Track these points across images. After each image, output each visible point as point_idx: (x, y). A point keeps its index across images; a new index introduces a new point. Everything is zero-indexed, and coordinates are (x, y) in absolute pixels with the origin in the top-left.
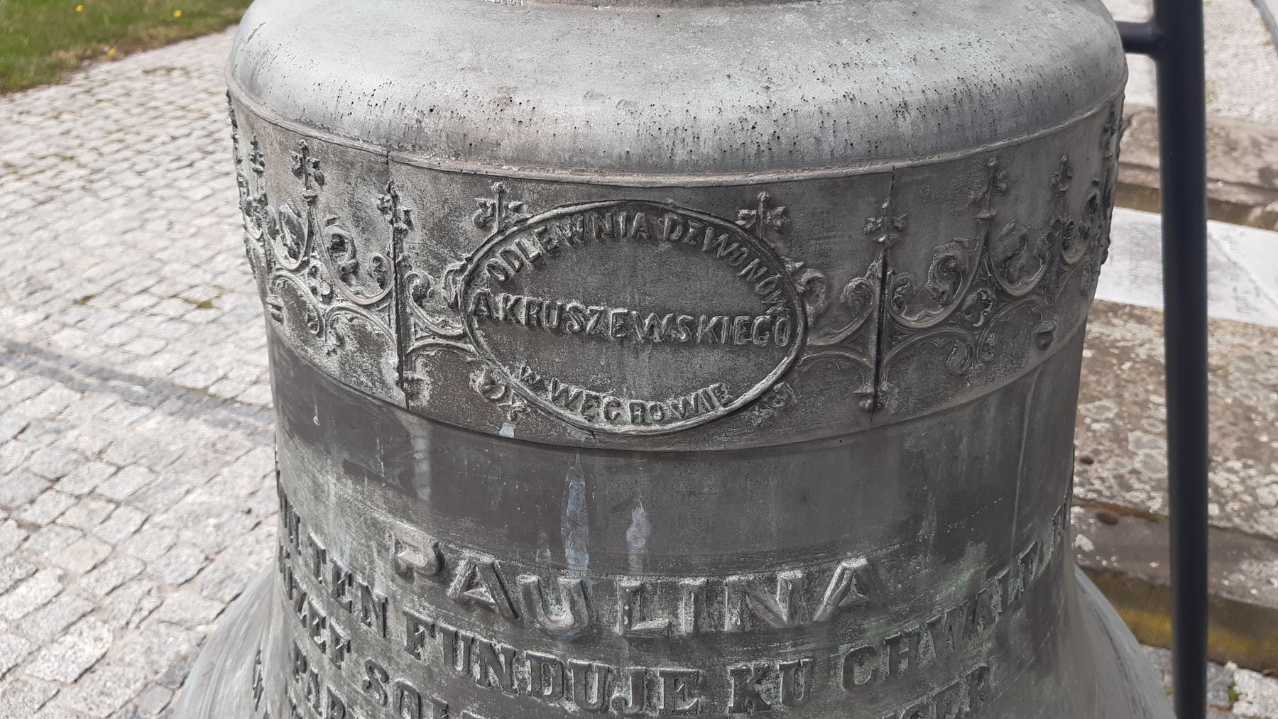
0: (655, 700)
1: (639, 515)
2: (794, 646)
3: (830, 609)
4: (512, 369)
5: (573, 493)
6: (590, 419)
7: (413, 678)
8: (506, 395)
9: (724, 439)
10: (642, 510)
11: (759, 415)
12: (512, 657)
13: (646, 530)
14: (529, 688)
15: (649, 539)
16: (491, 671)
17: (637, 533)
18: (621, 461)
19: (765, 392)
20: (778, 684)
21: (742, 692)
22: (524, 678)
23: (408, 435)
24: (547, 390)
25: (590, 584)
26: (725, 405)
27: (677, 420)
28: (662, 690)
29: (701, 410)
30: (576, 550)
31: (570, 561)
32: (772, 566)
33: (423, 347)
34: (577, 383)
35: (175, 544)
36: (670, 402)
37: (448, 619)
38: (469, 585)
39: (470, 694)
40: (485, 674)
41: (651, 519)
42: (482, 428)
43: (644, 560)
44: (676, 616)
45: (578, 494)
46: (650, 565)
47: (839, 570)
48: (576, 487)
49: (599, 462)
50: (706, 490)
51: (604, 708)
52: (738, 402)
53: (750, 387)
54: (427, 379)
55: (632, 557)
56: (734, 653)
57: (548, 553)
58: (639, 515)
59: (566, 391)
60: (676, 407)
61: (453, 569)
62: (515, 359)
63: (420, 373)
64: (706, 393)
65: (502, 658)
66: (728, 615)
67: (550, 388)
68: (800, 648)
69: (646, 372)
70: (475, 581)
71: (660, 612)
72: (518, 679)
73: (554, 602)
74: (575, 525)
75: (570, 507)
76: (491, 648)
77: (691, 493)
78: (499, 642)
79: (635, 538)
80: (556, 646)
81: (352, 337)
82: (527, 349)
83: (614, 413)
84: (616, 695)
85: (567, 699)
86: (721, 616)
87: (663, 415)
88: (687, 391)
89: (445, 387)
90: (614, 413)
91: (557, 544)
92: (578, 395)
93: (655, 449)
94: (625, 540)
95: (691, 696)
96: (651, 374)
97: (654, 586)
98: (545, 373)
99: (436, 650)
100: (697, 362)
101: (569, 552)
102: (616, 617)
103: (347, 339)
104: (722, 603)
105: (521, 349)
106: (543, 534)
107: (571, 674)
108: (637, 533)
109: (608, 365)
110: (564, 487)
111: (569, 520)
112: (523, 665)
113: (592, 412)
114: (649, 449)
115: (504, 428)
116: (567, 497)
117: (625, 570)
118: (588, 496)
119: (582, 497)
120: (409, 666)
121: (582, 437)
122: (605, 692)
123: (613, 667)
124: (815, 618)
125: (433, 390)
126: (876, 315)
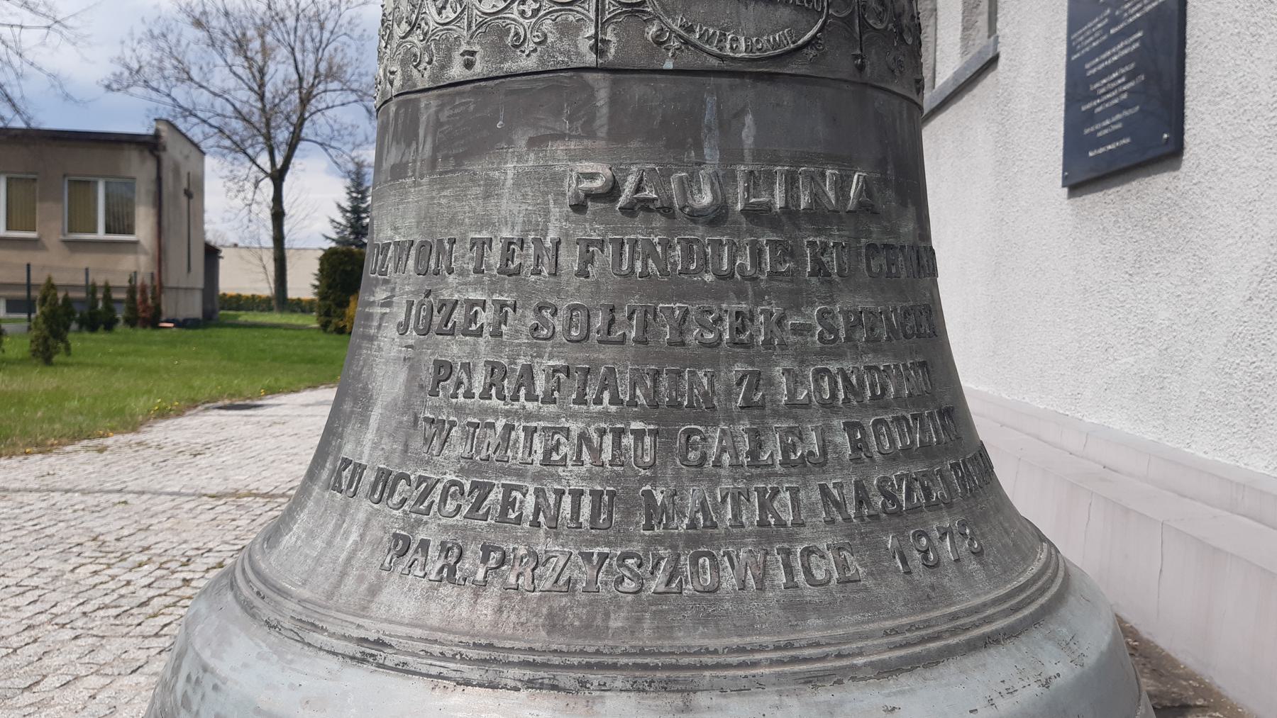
0: (763, 265)
1: (749, 119)
2: (838, 230)
3: (855, 201)
4: (674, 20)
5: (709, 106)
6: (721, 49)
7: (581, 298)
8: (669, 39)
9: (795, 66)
10: (751, 116)
11: (811, 53)
12: (667, 245)
13: (753, 132)
14: (679, 268)
15: (755, 137)
16: (650, 261)
17: (748, 135)
18: (738, 81)
19: (814, 37)
20: (833, 258)
21: (815, 260)
22: (675, 261)
23: (593, 88)
24: (694, 32)
25: (721, 174)
26: (793, 43)
27: (769, 50)
28: (768, 256)
29: (782, 45)
30: (711, 149)
31: (707, 157)
32: (822, 164)
33: (613, 17)
34: (712, 26)
35: (147, 662)
36: (765, 38)
37: (614, 231)
38: (638, 189)
39: (633, 289)
40: (645, 265)
41: (756, 122)
42: (651, 67)
43: (753, 153)
44: (773, 196)
45: (712, 107)
46: (757, 155)
47: (856, 177)
48: (711, 101)
49: (725, 81)
50: (785, 103)
51: (731, 275)
52: (800, 42)
53: (805, 34)
54: (614, 39)
55: (746, 151)
56: (807, 229)
57: (693, 153)
58: (749, 119)
59: (707, 30)
60: (769, 41)
61: (623, 185)
62: (675, 14)
63: (610, 36)
64: (783, 34)
65: (659, 249)
66: (802, 197)
67: (698, 30)
68: (842, 233)
69: (752, 19)
70: (642, 185)
71: (763, 193)
72: (671, 263)
73: (697, 192)
74: (710, 129)
75: (707, 117)
76: (650, 242)
77: (778, 105)
78: (656, 236)
79: (747, 137)
80: (698, 229)
81: (554, 31)
82: (683, 6)
83: (734, 46)
84: (738, 262)
85: (706, 272)
86: (798, 198)
87: (762, 46)
88: (774, 32)
89: (627, 41)
90: (734, 46)
91: (698, 146)
92: (714, 33)
93: (759, 70)
94: (741, 138)
95: (785, 262)
96: (755, 20)
97: (760, 172)
98: (694, 21)
99: (605, 263)
100: (778, 13)
101: (706, 151)
102: (737, 198)
103: (549, 34)
104: (798, 188)
105: (680, 7)
106: (690, 140)
107: (709, 250)
108: (748, 135)
109: (731, 13)
110: (703, 102)
111: (707, 126)
112: (674, 250)
113: (721, 44)
114: (755, 70)
115: (667, 63)
116: (705, 109)
117: (741, 160)
118: (718, 107)
119: (715, 108)
120: (578, 289)
121: (715, 63)
122: (732, 261)
123: (736, 240)
124: (848, 209)
125: (618, 46)
126: (856, 8)
